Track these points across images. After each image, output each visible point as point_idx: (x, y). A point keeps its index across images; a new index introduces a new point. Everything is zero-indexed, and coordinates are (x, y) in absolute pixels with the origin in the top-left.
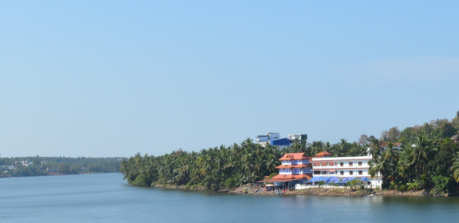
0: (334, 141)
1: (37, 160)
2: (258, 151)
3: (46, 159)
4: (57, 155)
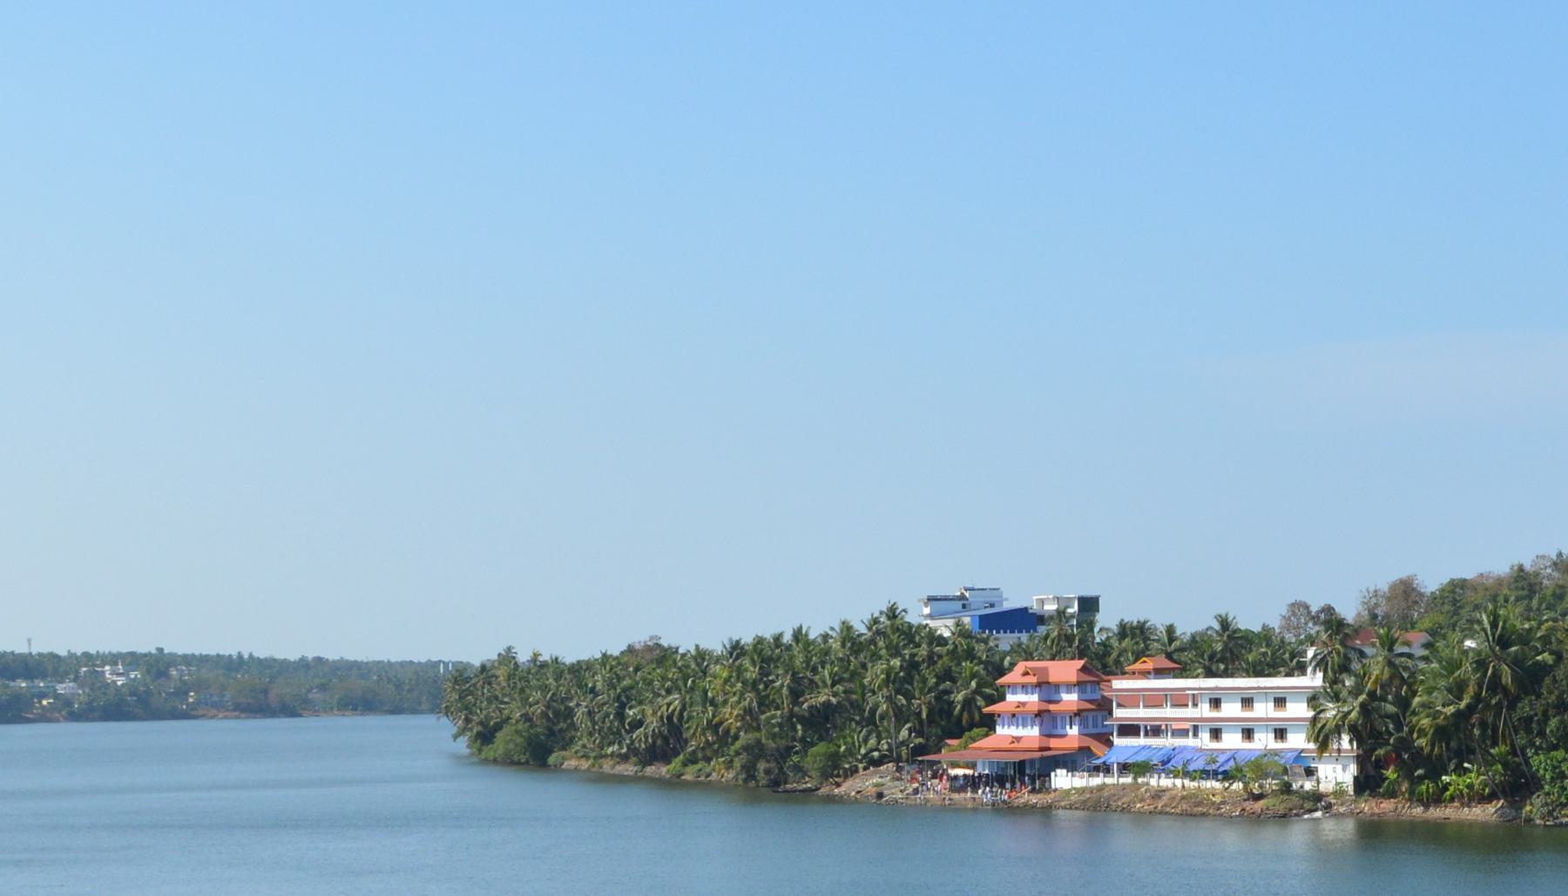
0: (1193, 620)
1: (158, 664)
2: (923, 651)
3: (188, 660)
4: (229, 649)
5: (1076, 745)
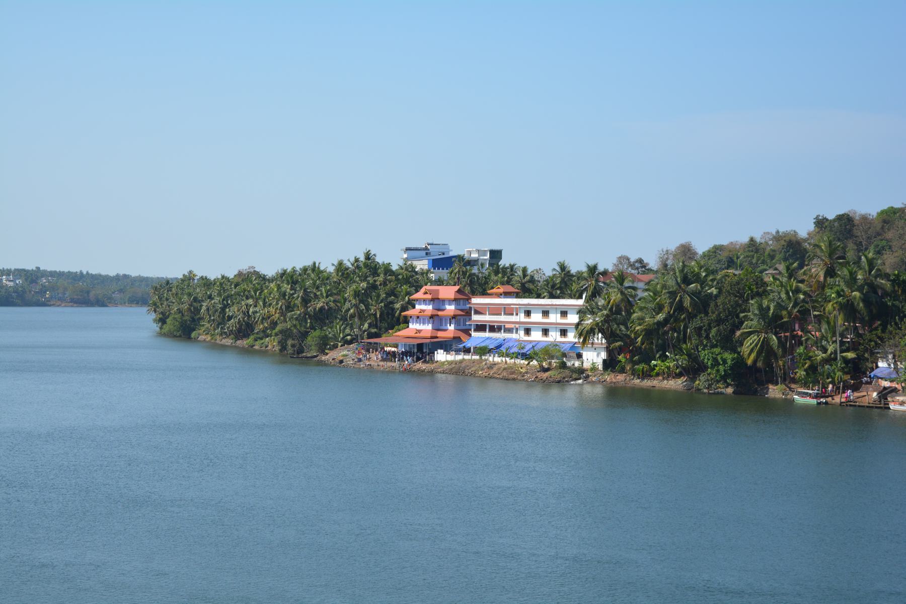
1: (32, 276)
2: (381, 278)
3: (53, 274)
4: (75, 269)
5: (452, 336)
